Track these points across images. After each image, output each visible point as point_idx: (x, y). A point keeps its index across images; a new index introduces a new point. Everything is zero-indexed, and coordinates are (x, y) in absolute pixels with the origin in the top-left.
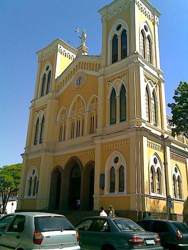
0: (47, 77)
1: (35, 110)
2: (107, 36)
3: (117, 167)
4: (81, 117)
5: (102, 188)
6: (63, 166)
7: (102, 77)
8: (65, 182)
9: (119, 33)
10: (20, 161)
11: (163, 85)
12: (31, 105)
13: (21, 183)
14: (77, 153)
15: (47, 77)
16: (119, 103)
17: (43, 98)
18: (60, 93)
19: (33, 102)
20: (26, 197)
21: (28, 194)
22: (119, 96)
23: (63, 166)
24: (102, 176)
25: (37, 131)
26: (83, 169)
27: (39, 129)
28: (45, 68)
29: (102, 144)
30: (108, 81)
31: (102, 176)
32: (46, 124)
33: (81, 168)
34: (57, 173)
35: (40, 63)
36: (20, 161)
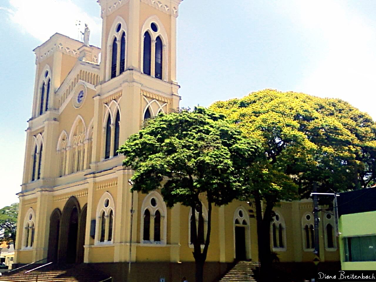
0: (46, 88)
1: (32, 133)
2: (107, 40)
3: (107, 211)
4: (77, 147)
5: (93, 236)
6: (62, 209)
7: (98, 97)
8: (63, 229)
9: (119, 36)
10: (17, 200)
11: (35, 281)
12: (27, 125)
13: (18, 228)
14: (78, 191)
15: (46, 88)
16: (152, 62)
17: (41, 116)
18: (62, 109)
19: (30, 122)
20: (23, 248)
21: (32, 180)
22: (114, 123)
23: (62, 209)
24: (93, 222)
25: (42, 100)
26: (80, 212)
27: (37, 160)
28: (44, 74)
29: (95, 183)
30: (104, 103)
31: (93, 222)
32: (43, 152)
33: (78, 210)
34: (56, 217)
35: (38, 65)
36: (17, 200)
